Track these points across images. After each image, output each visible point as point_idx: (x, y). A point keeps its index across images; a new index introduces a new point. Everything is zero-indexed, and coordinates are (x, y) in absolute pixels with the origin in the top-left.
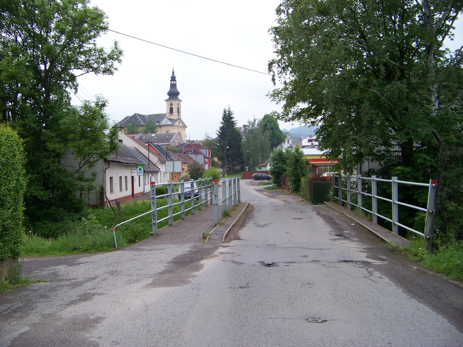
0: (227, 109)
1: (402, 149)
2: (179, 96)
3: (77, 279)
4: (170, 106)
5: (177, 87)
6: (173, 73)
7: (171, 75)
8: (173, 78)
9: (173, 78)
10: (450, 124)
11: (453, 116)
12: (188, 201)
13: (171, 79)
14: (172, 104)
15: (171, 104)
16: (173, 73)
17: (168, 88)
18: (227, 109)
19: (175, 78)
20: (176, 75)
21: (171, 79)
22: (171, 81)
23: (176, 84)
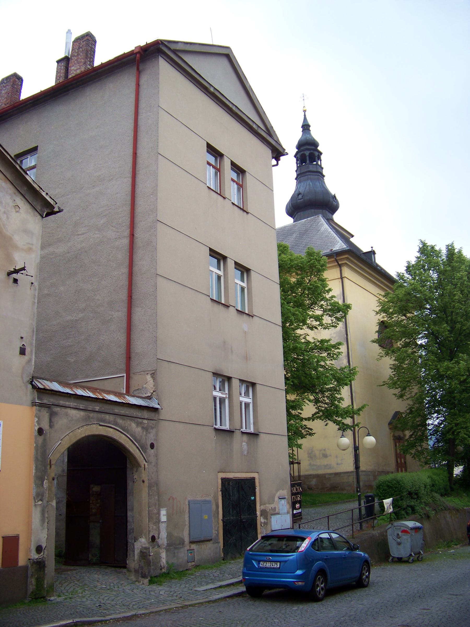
6: (306, 127)
16: (306, 127)
20: (315, 133)
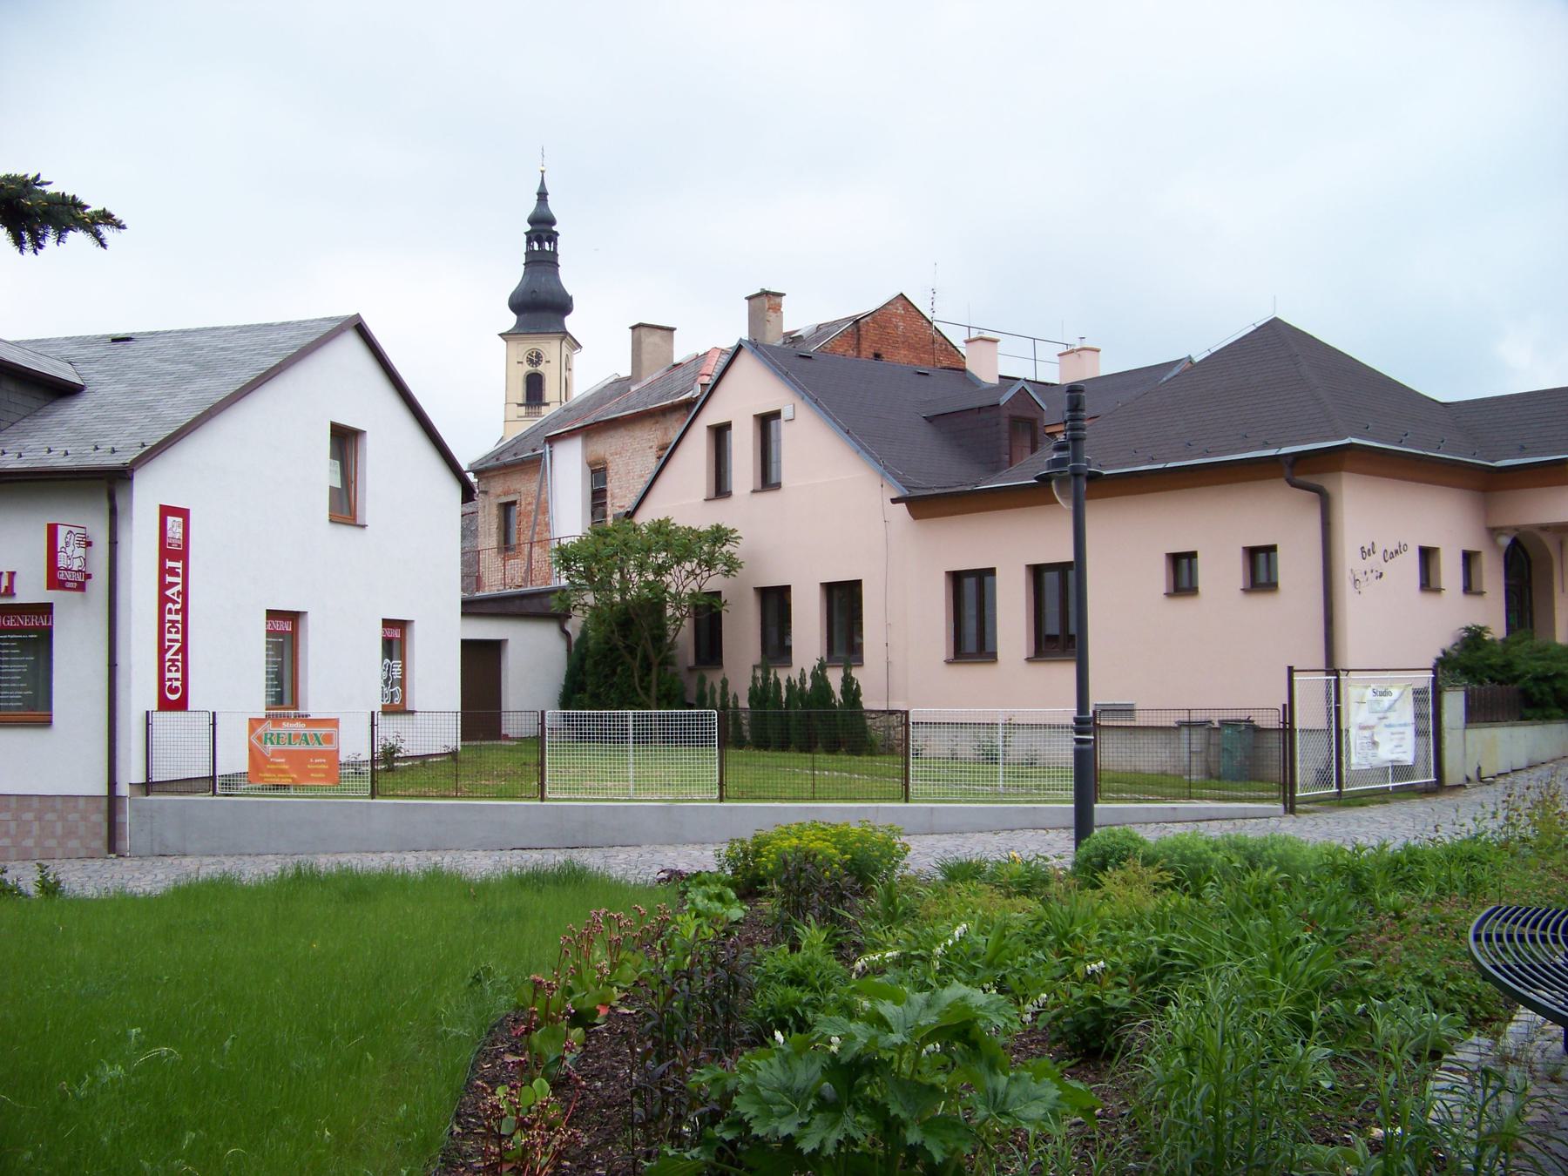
0: (29, 253)
1: (865, 723)
2: (570, 322)
3: (1124, 824)
4: (528, 368)
5: (562, 272)
6: (542, 195)
7: (531, 205)
8: (542, 228)
9: (542, 228)
10: (468, 1133)
11: (1396, 935)
12: (447, 805)
13: (528, 228)
14: (539, 356)
15: (535, 358)
16: (542, 195)
17: (512, 274)
18: (29, 253)
19: (552, 222)
20: (553, 206)
21: (528, 228)
22: (530, 237)
23: (555, 254)
